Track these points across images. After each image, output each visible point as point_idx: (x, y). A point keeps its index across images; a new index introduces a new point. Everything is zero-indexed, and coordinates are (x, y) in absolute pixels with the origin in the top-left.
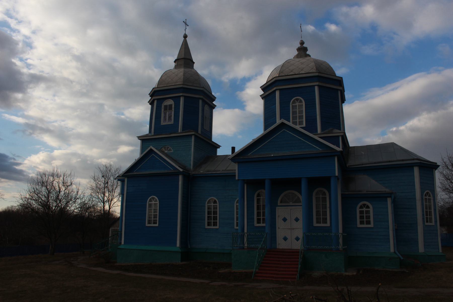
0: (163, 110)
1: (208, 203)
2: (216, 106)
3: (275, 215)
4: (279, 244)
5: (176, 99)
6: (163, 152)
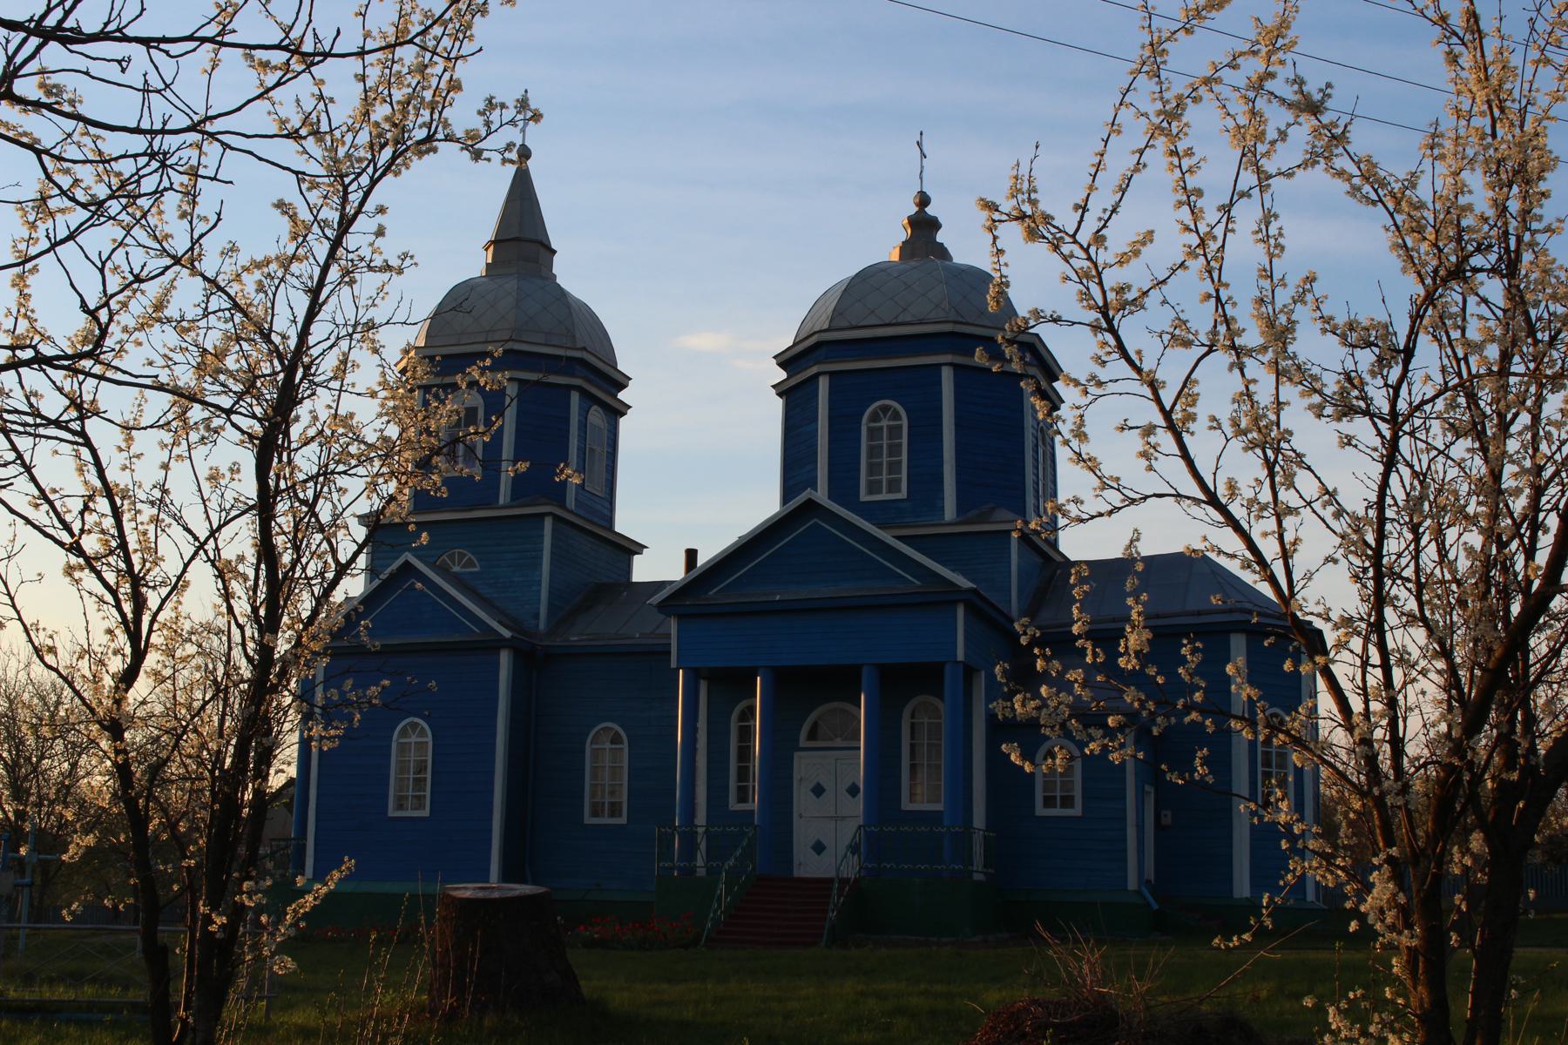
2: (629, 407)
3: (791, 777)
4: (800, 864)
6: (444, 571)
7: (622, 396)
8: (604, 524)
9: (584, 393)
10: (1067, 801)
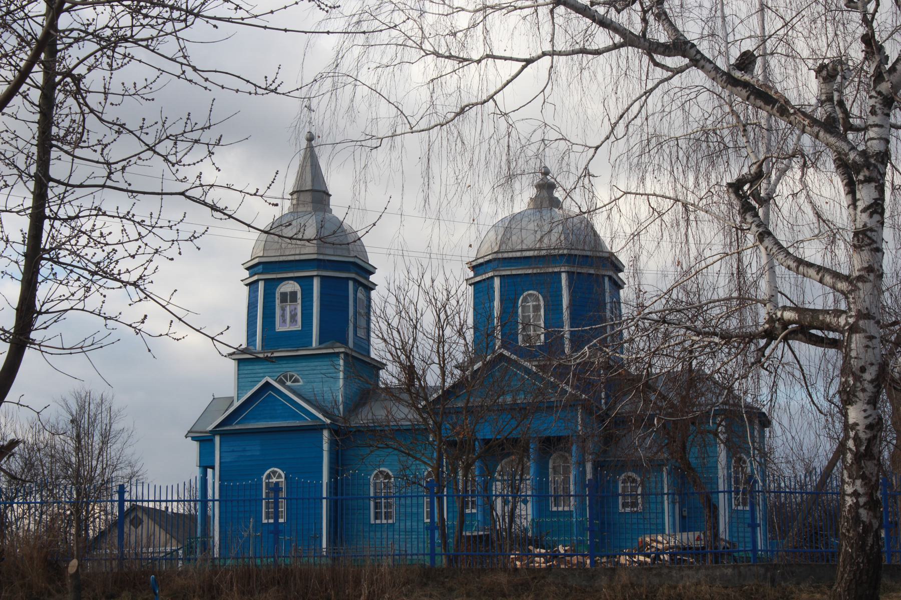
0: (278, 301)
5: (307, 283)
7: (372, 278)
8: (366, 354)
9: (355, 280)
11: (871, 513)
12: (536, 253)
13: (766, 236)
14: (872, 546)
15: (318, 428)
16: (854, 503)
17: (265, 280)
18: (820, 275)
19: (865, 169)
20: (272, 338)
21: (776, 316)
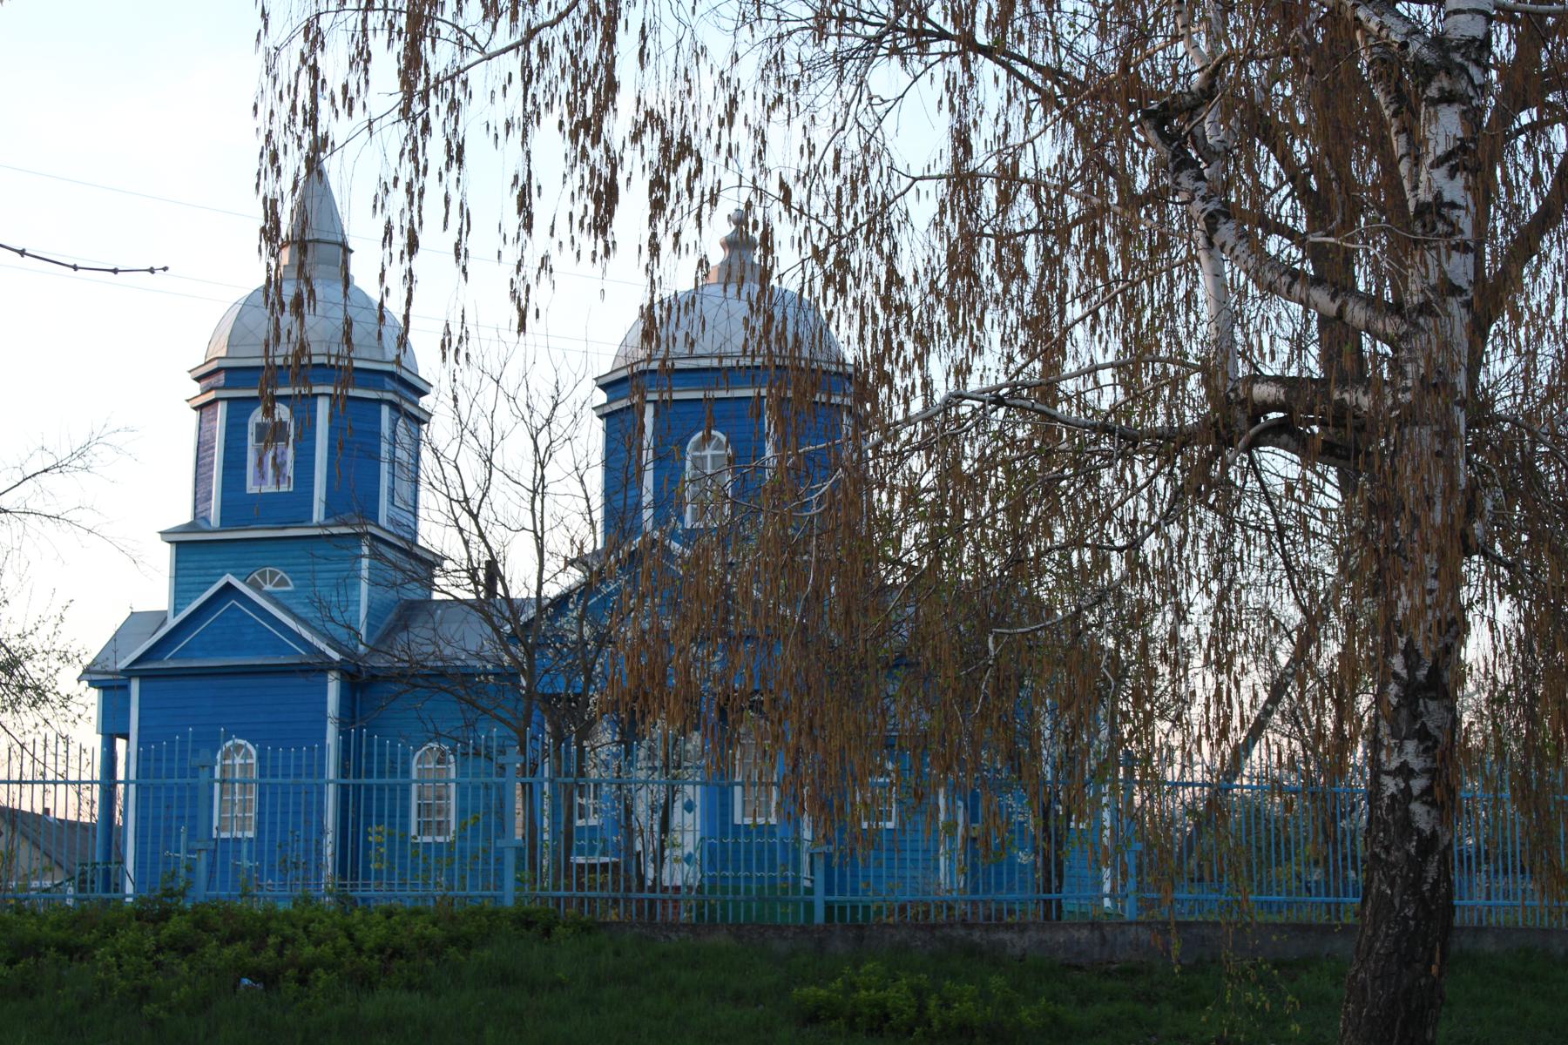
1: (419, 762)
5: (304, 407)
7: (424, 402)
9: (392, 404)
10: (441, 828)
11: (1434, 813)
12: (715, 363)
13: (1223, 220)
14: (1436, 884)
15: (317, 669)
16: (1401, 791)
17: (228, 399)
18: (1338, 302)
19: (1442, 74)
20: (237, 506)
21: (1237, 395)
